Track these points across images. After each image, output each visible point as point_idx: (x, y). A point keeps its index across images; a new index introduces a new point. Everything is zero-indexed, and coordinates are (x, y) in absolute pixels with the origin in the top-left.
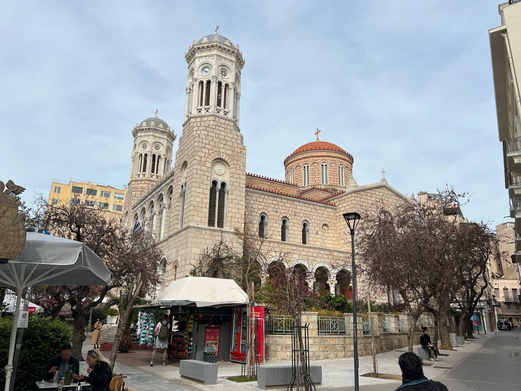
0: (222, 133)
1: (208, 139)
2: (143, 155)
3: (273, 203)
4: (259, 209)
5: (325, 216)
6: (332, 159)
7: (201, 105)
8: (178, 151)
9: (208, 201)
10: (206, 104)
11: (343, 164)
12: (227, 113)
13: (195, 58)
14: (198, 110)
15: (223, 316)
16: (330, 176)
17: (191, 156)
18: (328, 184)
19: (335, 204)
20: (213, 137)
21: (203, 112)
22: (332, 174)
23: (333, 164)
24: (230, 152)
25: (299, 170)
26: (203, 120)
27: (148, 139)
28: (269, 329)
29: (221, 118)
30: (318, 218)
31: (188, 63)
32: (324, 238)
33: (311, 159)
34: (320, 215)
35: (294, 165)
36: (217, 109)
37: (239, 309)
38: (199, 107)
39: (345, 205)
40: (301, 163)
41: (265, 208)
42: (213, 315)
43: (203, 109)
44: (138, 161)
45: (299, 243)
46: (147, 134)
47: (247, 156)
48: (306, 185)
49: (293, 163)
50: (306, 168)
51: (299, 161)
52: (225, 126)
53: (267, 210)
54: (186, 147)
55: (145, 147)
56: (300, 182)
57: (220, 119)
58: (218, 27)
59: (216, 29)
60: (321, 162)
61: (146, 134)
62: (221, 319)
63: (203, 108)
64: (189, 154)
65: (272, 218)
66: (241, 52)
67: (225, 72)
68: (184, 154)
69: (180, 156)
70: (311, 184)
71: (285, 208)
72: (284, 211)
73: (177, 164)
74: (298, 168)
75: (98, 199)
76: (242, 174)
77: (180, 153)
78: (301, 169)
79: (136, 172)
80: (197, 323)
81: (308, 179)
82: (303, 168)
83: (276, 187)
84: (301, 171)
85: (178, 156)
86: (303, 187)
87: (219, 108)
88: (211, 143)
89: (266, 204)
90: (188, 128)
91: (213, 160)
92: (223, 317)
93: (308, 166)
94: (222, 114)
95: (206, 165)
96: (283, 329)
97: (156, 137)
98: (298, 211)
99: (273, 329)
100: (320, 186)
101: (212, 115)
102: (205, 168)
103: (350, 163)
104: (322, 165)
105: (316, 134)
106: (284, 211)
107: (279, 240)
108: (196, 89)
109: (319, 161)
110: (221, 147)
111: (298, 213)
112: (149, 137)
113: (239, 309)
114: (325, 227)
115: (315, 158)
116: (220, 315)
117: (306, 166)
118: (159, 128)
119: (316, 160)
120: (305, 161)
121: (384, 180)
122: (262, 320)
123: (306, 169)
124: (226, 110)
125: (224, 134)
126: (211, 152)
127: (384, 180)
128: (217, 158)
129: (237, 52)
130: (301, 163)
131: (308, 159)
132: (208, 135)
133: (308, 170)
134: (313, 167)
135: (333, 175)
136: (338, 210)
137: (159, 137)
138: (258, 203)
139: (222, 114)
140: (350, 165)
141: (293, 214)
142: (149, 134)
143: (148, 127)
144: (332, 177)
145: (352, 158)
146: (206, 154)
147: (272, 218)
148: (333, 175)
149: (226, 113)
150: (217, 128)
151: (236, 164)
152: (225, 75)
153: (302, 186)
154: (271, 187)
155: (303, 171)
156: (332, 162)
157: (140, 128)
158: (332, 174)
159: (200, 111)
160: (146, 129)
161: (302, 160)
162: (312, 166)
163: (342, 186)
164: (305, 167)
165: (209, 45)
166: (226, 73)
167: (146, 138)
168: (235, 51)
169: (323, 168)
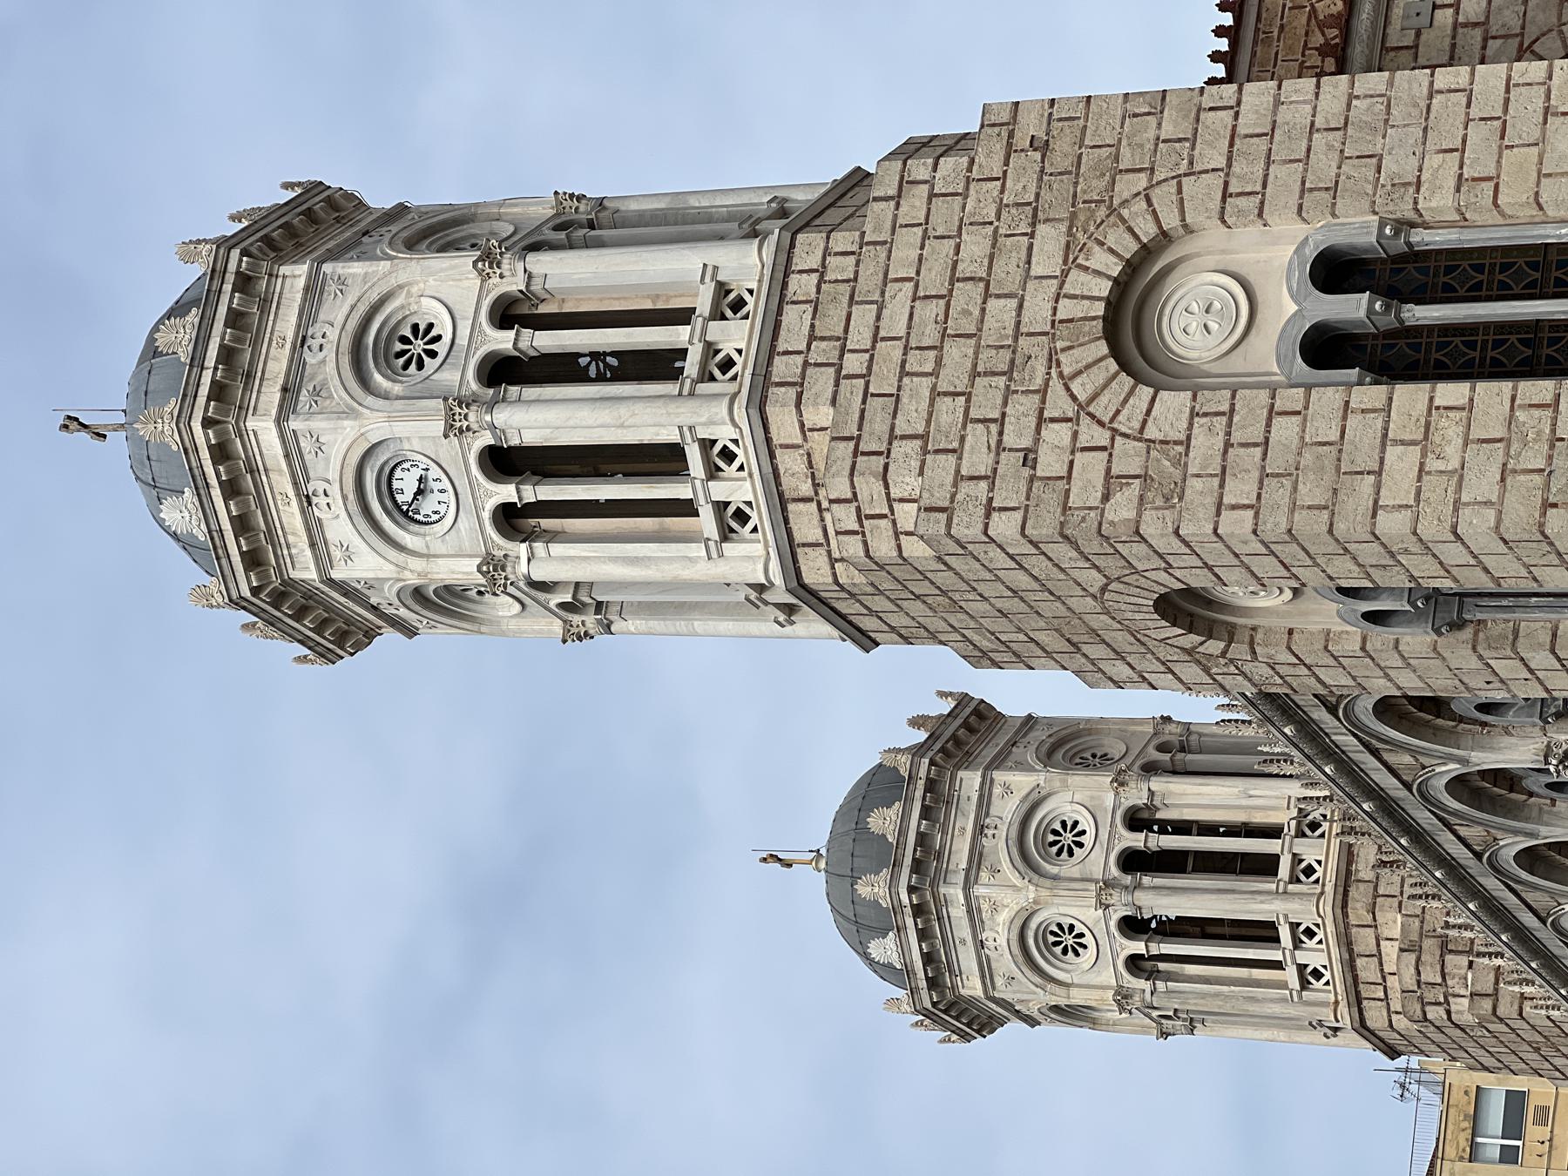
0: (895, 323)
7: (686, 508)
8: (1077, 673)
10: (674, 466)
12: (722, 289)
13: (331, 583)
14: (726, 534)
21: (739, 489)
24: (1050, 240)
26: (806, 489)
27: (1003, 917)
31: (370, 634)
36: (701, 379)
38: (706, 521)
43: (719, 491)
46: (965, 922)
47: (1070, 88)
54: (1042, 607)
55: (1069, 940)
57: (781, 347)
58: (71, 423)
59: (84, 436)
61: (962, 930)
63: (1293, 957)
64: (1094, 580)
66: (235, 218)
67: (404, 340)
69: (1120, 656)
73: (1191, 672)
76: (1227, 116)
79: (1284, 1000)
87: (691, 366)
90: (879, 603)
94: (735, 336)
97: (977, 858)
101: (1339, 911)
102: (1206, 444)
110: (1009, 319)
112: (985, 907)
118: (902, 832)
124: (704, 304)
126: (1058, 403)
128: (1102, 348)
129: (235, 253)
132: (924, 437)
137: (980, 830)
139: (735, 336)
142: (958, 912)
143: (910, 921)
146: (1083, 441)
149: (728, 303)
152: (426, 332)
157: (923, 984)
159: (732, 520)
160: (923, 935)
165: (213, 481)
166: (415, 328)
167: (999, 934)
168: (232, 267)
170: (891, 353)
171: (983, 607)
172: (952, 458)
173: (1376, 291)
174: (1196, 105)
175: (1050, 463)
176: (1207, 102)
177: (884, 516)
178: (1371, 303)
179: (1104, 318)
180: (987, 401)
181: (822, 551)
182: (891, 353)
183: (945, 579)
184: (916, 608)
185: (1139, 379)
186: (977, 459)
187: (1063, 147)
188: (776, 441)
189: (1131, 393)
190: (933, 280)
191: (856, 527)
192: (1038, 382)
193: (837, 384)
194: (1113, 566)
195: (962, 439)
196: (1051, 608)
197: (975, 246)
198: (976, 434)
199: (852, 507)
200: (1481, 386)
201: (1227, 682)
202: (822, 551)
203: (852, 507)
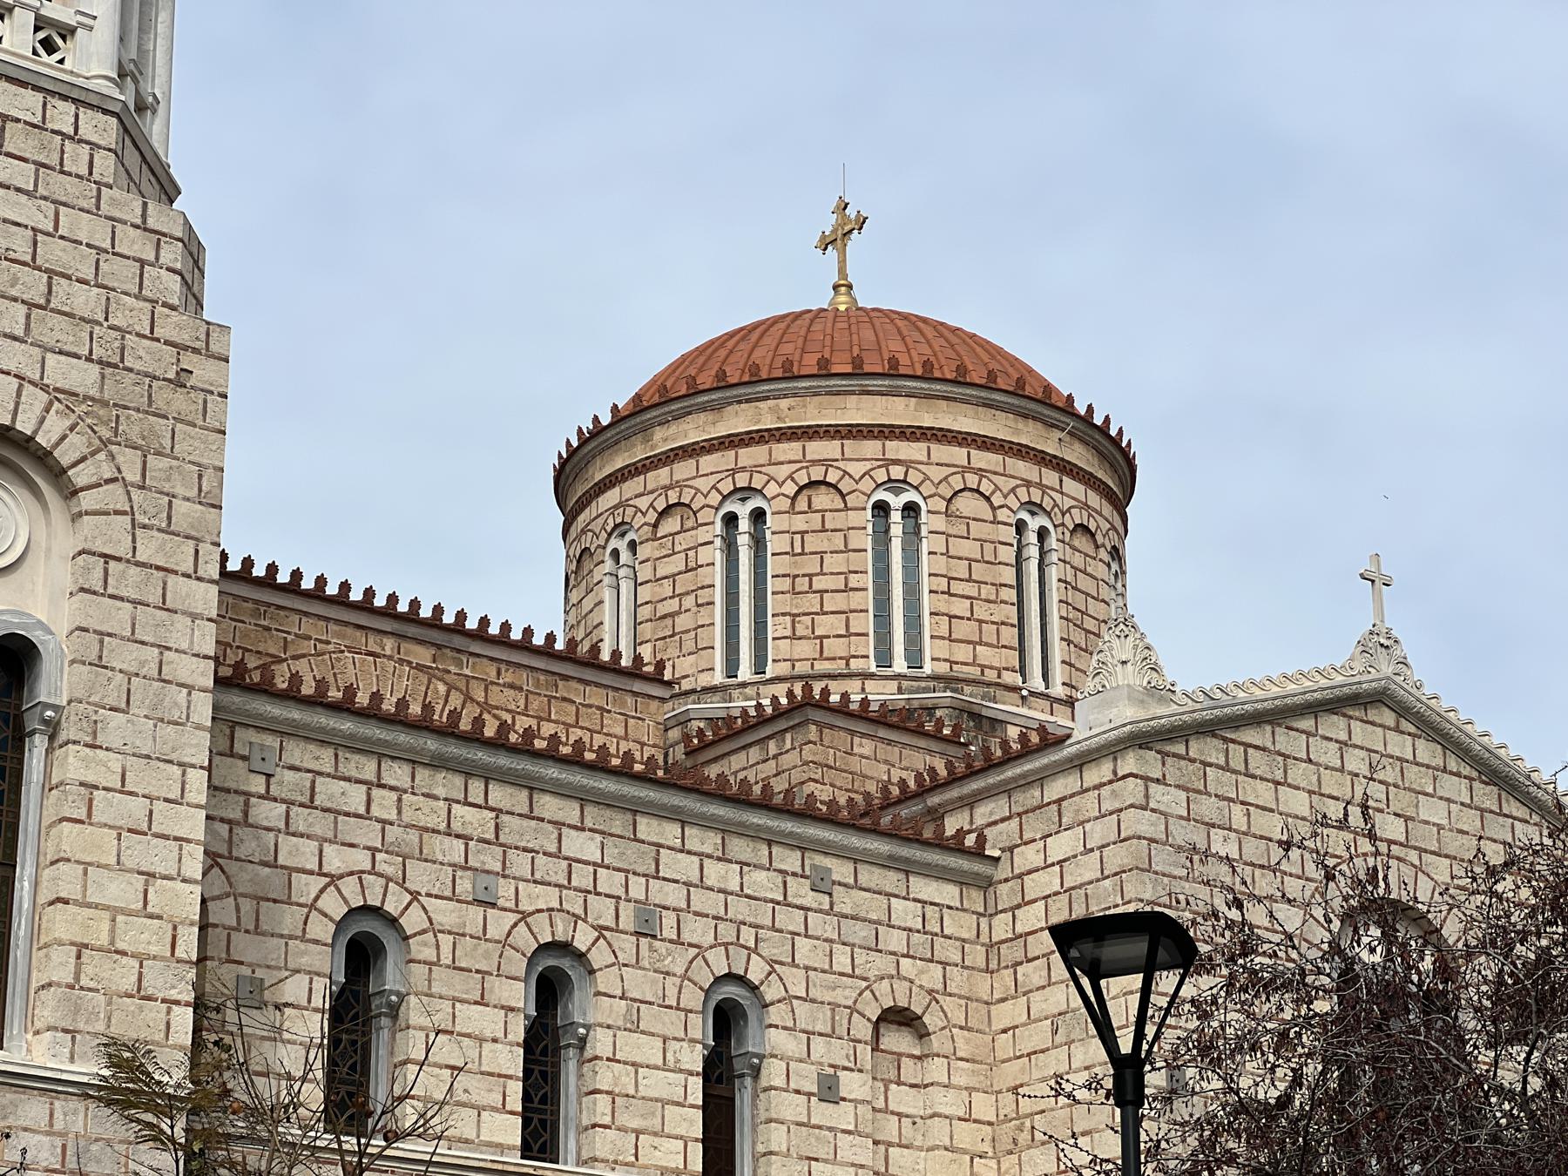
5: (895, 940)
6: (958, 454)
11: (1047, 504)
16: (942, 604)
18: (928, 669)
19: (981, 840)
22: (957, 587)
23: (968, 505)
24: (83, 377)
25: (683, 541)
30: (842, 961)
32: (890, 1129)
34: (861, 933)
35: (643, 503)
39: (1061, 845)
47: (235, 415)
48: (745, 672)
50: (744, 525)
51: (684, 469)
56: (689, 645)
60: (866, 485)
65: (446, 959)
71: (555, 870)
72: (549, 897)
74: (671, 525)
78: (703, 535)
82: (718, 527)
84: (704, 555)
89: (393, 833)
93: (758, 516)
104: (882, 509)
106: (549, 897)
107: (501, 1148)
109: (856, 469)
111: (669, 919)
114: (897, 1040)
115: (820, 449)
117: (743, 511)
119: (826, 463)
120: (734, 472)
121: (1380, 642)
123: (743, 540)
127: (1380, 642)
130: (704, 484)
133: (758, 543)
134: (799, 523)
135: (970, 589)
140: (1107, 509)
144: (961, 608)
147: (446, 959)
148: (970, 589)
153: (705, 680)
154: (442, 688)
155: (718, 557)
158: (957, 587)
162: (792, 510)
163: (1037, 683)
164: (731, 520)
169: (882, 536)
176: (205, 548)
187: (178, 402)
190: (51, 253)
197: (85, 300)
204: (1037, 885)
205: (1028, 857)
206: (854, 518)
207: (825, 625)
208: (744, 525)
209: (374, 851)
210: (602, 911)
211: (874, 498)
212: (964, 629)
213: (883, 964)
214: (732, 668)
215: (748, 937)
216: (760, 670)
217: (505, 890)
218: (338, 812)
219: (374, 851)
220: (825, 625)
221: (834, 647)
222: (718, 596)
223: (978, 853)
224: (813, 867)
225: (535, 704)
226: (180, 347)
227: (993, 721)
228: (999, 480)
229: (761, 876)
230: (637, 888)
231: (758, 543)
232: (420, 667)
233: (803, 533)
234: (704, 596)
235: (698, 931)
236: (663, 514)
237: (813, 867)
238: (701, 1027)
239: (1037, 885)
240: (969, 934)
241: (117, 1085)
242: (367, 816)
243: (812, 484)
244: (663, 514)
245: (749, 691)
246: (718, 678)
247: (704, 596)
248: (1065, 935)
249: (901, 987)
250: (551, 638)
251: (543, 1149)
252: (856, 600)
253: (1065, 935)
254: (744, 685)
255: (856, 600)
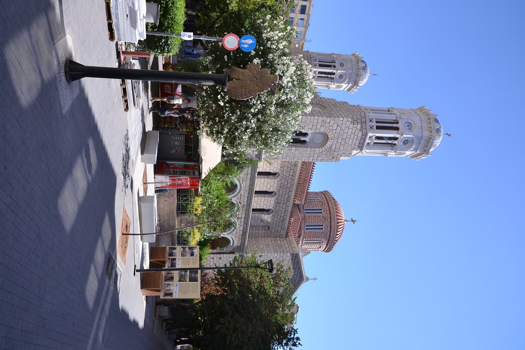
1: (346, 129)
2: (334, 64)
3: (288, 184)
4: (283, 172)
5: (277, 228)
6: (328, 234)
8: (336, 101)
9: (258, 208)
15: (192, 154)
16: (313, 232)
17: (330, 113)
18: (306, 230)
19: (287, 237)
20: (347, 133)
22: (314, 234)
23: (323, 235)
24: (333, 148)
25: (319, 205)
26: (363, 124)
28: (181, 191)
29: (364, 140)
30: (275, 222)
31: (417, 109)
32: (258, 227)
33: (329, 216)
34: (277, 224)
35: (323, 200)
37: (197, 167)
39: (286, 245)
40: (325, 207)
41: (284, 177)
42: (192, 146)
44: (329, 59)
45: (253, 206)
47: (330, 163)
48: (305, 211)
49: (325, 199)
50: (321, 211)
51: (327, 205)
52: (357, 144)
53: (282, 178)
54: (339, 109)
56: (308, 205)
58: (449, 135)
59: (449, 134)
62: (189, 153)
64: (333, 112)
65: (275, 183)
68: (333, 107)
69: (331, 102)
70: (306, 215)
71: (284, 193)
72: (281, 193)
73: (323, 100)
74: (321, 203)
75: (296, 16)
76: (314, 159)
77: (333, 103)
78: (320, 207)
80: (186, 133)
81: (310, 213)
83: (303, 186)
85: (331, 101)
86: (304, 208)
88: (342, 132)
89: (288, 177)
90: (356, 110)
91: (327, 133)
92: (191, 154)
95: (322, 127)
96: (181, 195)
98: (281, 206)
99: (181, 193)
100: (304, 223)
102: (319, 126)
103: (324, 250)
105: (352, 219)
106: (281, 193)
107: (256, 189)
108: (392, 118)
109: (327, 223)
110: (338, 140)
111: (279, 205)
113: (197, 167)
114: (267, 228)
115: (329, 219)
116: (193, 152)
119: (327, 220)
121: (307, 279)
122: (188, 186)
125: (350, 143)
126: (334, 131)
127: (307, 279)
128: (329, 137)
130: (325, 207)
131: (329, 213)
133: (319, 213)
134: (321, 217)
135: (314, 235)
136: (282, 239)
138: (288, 171)
140: (323, 249)
141: (278, 201)
144: (312, 234)
145: (329, 251)
146: (332, 127)
147: (275, 183)
148: (314, 235)
150: (356, 137)
151: (323, 153)
153: (304, 207)
154: (303, 181)
156: (325, 234)
158: (314, 234)
161: (327, 207)
162: (322, 216)
163: (304, 242)
164: (321, 210)
169: (320, 226)
170: (352, 138)
171: (345, 109)
172: (346, 126)
173: (300, 140)
174: (317, 160)
175: (335, 125)
176: (316, 160)
177: (355, 120)
178: (301, 139)
179: (328, 139)
180: (342, 132)
181: (362, 117)
182: (352, 138)
183: (349, 113)
184: (352, 109)
185: (325, 133)
186: (343, 126)
187: (331, 157)
188: (365, 129)
189: (326, 132)
190: (346, 145)
191: (358, 120)
192: (336, 134)
193: (358, 135)
194: (330, 113)
195: (345, 128)
196: (338, 109)
197: (341, 148)
198: (344, 129)
199: (358, 122)
200: (259, 190)
201: (320, 99)
202: (362, 117)
203: (358, 122)
204: (282, 243)
205: (285, 242)
206: (321, 223)
207: (310, 220)
208: (321, 211)
209: (286, 176)
210: (280, 198)
211: (324, 225)
212: (310, 234)
213: (274, 227)
214: (306, 210)
215: (277, 213)
216: (306, 213)
217: (282, 189)
218: (290, 172)
219: (286, 176)
220: (310, 220)
221: (308, 221)
222: (313, 208)
223: (286, 237)
224: (284, 220)
225: (301, 190)
226: (337, 157)
227: (300, 237)
228: (326, 238)
229: (283, 214)
230: (282, 202)
231: (319, 213)
232: (305, 179)
233: (320, 217)
234: (313, 207)
235: (278, 208)
236: (322, 203)
237: (284, 220)
238: (268, 208)
239: (282, 243)
240: (277, 235)
241: (236, 301)
242: (289, 175)
243: (325, 218)
244: (322, 203)
245: (303, 212)
246: (305, 208)
247: (313, 207)
248: (271, 260)
249: (272, 228)
250: (309, 190)
251: (256, 193)
252: (313, 223)
253: (271, 260)
254: (304, 211)
255: (313, 223)
